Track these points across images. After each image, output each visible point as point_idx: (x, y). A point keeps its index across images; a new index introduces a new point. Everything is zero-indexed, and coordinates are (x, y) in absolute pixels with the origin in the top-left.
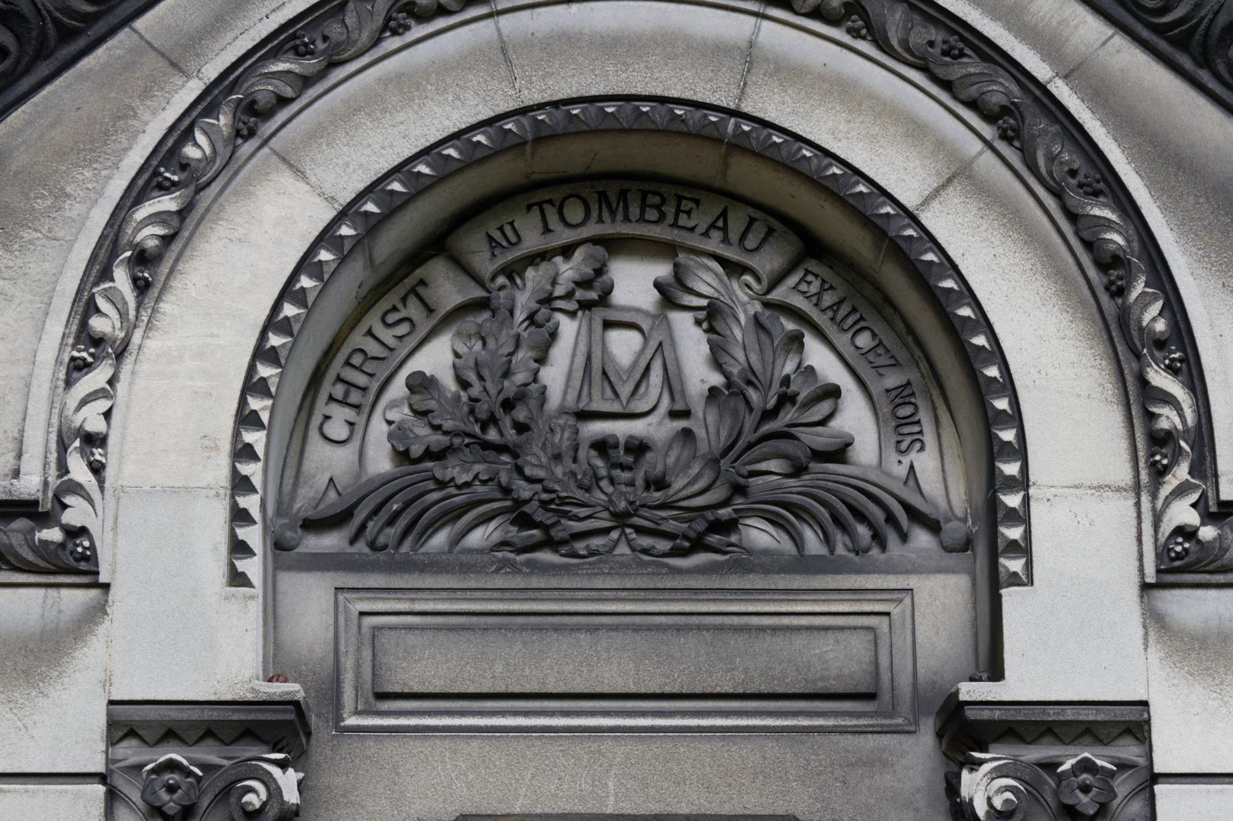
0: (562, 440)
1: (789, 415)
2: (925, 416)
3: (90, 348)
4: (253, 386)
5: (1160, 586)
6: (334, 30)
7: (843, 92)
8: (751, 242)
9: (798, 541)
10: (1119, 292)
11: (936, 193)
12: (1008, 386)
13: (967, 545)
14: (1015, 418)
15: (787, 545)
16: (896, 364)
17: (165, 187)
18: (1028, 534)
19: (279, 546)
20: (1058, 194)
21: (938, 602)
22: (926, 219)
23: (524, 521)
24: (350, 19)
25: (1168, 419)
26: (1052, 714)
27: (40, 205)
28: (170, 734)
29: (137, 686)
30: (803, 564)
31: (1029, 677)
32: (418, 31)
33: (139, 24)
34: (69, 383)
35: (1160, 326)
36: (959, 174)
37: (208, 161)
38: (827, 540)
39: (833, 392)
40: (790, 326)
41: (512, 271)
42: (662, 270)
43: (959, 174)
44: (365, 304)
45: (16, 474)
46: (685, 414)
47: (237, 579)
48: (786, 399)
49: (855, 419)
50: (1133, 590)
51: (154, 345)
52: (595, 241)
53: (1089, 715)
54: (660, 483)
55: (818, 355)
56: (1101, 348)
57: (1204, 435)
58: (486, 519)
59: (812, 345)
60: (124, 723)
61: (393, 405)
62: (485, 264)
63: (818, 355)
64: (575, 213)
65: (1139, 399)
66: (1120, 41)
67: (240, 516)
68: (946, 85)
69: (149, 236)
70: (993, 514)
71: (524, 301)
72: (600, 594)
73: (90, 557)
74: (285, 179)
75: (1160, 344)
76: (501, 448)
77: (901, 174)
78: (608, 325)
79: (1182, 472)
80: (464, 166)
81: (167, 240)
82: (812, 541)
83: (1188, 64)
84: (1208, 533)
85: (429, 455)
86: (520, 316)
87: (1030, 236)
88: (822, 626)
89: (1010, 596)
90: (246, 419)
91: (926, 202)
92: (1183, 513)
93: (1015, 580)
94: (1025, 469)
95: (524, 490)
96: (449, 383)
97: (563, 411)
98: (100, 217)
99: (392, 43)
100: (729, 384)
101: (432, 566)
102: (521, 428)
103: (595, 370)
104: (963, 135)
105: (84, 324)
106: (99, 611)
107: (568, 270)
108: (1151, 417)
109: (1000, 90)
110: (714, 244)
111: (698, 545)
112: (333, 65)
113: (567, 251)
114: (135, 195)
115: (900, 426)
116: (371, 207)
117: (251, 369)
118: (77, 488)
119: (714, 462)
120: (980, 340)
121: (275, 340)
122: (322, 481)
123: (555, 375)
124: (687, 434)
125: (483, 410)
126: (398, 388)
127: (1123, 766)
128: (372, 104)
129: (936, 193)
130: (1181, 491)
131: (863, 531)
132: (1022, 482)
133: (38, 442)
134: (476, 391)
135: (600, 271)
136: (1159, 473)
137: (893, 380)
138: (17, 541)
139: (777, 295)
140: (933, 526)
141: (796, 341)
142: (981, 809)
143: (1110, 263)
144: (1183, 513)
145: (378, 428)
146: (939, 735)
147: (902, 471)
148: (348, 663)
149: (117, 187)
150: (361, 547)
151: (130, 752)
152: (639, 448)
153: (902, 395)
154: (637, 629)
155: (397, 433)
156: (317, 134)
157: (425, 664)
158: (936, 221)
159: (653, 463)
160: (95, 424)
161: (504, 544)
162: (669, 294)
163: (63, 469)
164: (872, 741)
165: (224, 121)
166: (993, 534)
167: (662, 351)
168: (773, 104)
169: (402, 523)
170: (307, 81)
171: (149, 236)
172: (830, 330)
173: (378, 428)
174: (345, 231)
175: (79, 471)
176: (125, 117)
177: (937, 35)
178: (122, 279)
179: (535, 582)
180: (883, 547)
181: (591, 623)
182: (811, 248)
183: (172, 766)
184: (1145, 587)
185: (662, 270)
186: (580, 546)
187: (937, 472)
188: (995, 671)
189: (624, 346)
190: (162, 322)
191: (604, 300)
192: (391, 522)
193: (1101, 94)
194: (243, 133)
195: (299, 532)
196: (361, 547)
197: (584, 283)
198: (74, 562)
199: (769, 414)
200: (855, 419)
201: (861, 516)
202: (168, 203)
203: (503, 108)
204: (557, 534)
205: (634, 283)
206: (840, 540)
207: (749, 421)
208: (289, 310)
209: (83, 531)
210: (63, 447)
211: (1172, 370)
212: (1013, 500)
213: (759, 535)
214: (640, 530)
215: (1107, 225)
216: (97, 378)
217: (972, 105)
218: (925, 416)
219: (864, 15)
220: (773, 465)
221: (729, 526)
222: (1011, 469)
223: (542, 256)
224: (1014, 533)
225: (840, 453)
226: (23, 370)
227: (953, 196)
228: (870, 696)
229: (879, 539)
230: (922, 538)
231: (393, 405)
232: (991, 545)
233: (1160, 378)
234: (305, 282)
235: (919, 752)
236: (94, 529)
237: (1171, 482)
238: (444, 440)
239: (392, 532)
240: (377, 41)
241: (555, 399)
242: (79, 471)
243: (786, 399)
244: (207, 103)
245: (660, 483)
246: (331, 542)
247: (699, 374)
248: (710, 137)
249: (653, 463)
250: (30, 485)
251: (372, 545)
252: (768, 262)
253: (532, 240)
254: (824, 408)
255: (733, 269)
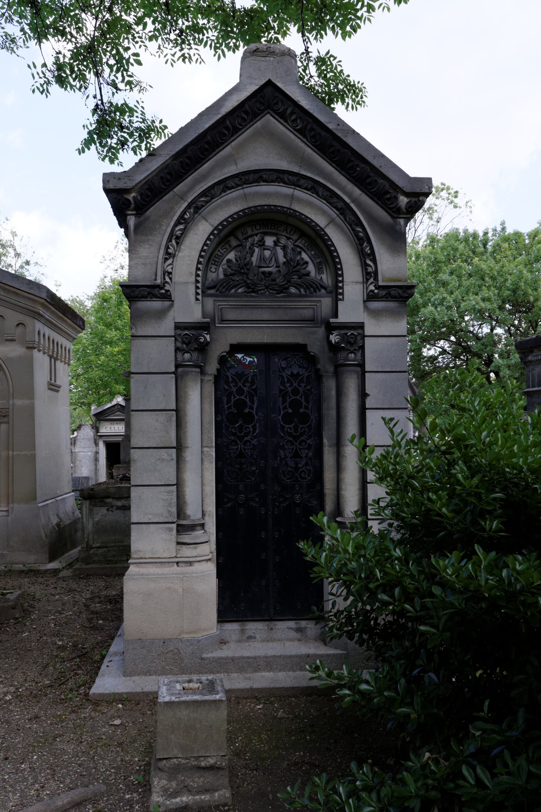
0: (256, 272)
1: (299, 267)
2: (324, 267)
3: (169, 256)
4: (199, 262)
5: (367, 301)
6: (213, 192)
7: (310, 204)
8: (292, 233)
9: (300, 291)
10: (362, 245)
11: (328, 225)
12: (340, 263)
13: (331, 292)
14: (341, 269)
15: (298, 292)
16: (319, 257)
17: (181, 224)
18: (343, 291)
19: (203, 292)
20: (351, 225)
21: (326, 302)
22: (326, 230)
23: (249, 288)
24: (216, 190)
25: (370, 269)
26: (347, 325)
27: (157, 227)
28: (186, 328)
29: (181, 319)
30: (301, 296)
31: (344, 317)
32: (228, 192)
33: (175, 190)
34: (165, 262)
35: (369, 252)
36: (332, 221)
37: (189, 218)
38: (306, 291)
39: (307, 263)
40: (299, 250)
41: (246, 239)
42: (274, 238)
43: (332, 221)
44: (218, 245)
45: (156, 280)
46: (279, 267)
47: (197, 299)
48: (298, 264)
49: (311, 268)
50: (362, 302)
51: (180, 254)
52: (262, 233)
53: (353, 325)
54: (274, 280)
55: (304, 256)
56: (358, 259)
57: (376, 273)
58: (241, 287)
59: (303, 253)
60: (178, 326)
61: (224, 265)
62: (241, 237)
63: (304, 256)
64: (258, 227)
65: (364, 266)
66: (363, 195)
67: (197, 288)
68: (330, 203)
69: (179, 233)
70: (337, 287)
71: (248, 245)
72: (263, 301)
73: (170, 296)
74: (204, 222)
75: (369, 255)
76: (244, 273)
77: (321, 221)
78: (264, 249)
79: (372, 280)
80: (237, 219)
81: (182, 234)
82: (302, 291)
83: (376, 199)
84: (376, 291)
85: (231, 275)
86: (247, 247)
87: (345, 234)
88: (304, 308)
89: (340, 303)
90: (198, 269)
91: (326, 227)
92: (372, 287)
93: (340, 300)
94: (343, 279)
95: (249, 282)
96: (234, 260)
97: (256, 266)
98: (169, 230)
99: (223, 194)
100: (287, 261)
101: (232, 296)
102: (248, 269)
103: (262, 258)
104: (333, 213)
105: (167, 251)
106: (172, 306)
107: (256, 239)
108: (367, 269)
109: (340, 205)
110: (284, 234)
111: (281, 292)
112: (212, 198)
113: (256, 235)
114: (176, 225)
115: (319, 270)
116: (220, 227)
117: (198, 259)
118: (167, 283)
119: (284, 276)
120: (335, 254)
121: (203, 254)
122: (210, 280)
123: (254, 259)
124: (279, 271)
125: (241, 266)
126: (225, 261)
127: (359, 334)
128: (220, 207)
129: (328, 225)
130: (372, 283)
131: (312, 289)
132: (342, 281)
133: (159, 273)
134: (239, 262)
135: (263, 239)
136: (368, 280)
137: (318, 260)
138: (156, 292)
139: (296, 244)
140: (325, 288)
141: (300, 253)
142: (333, 342)
143: (360, 239)
144: (372, 287)
145: (221, 269)
146: (325, 328)
147: (319, 278)
148: (216, 314)
149: (172, 224)
150: (218, 292)
151: (179, 332)
152: (270, 273)
153: (320, 263)
154: (270, 308)
155: (224, 270)
156: (210, 212)
157: (231, 315)
158: (328, 231)
159: (273, 276)
160: (170, 270)
161: (245, 292)
162: (276, 243)
163: (164, 279)
164: (313, 329)
165: (192, 210)
166: (337, 291)
167: (274, 254)
168: (297, 207)
169: (226, 288)
170: (207, 202)
171: (179, 233)
172: (307, 251)
173: (221, 269)
174: (215, 232)
175: (167, 279)
176: (172, 210)
177: (328, 193)
178: (174, 242)
179: (251, 299)
180: (316, 292)
181: (262, 307)
182: (303, 234)
183: (186, 334)
184: (364, 301)
185: (274, 238)
186: (259, 292)
187: (326, 278)
188: (336, 316)
189: (267, 253)
190: (181, 250)
191: (264, 244)
192: (224, 288)
193: (359, 205)
194: (196, 212)
195: (206, 289)
196: (218, 292)
197: (259, 241)
198: (167, 296)
199: (295, 267)
200: (311, 268)
201: (312, 287)
202: (182, 227)
203: (245, 207)
204: (255, 290)
205: (269, 241)
206: (308, 291)
207: (291, 268)
208: (205, 248)
209: (169, 291)
210: (164, 275)
211: (371, 260)
212: (340, 285)
213: (293, 290)
214: (271, 289)
215: (360, 232)
216: (170, 261)
217: (335, 207)
218: (324, 267)
219: (315, 189)
220: (296, 277)
221: (287, 288)
222: (340, 279)
223: (251, 236)
224: (341, 291)
225: (308, 274)
226: (155, 259)
227: (331, 226)
228: (313, 321)
229: (315, 291)
230: (323, 291)
231: (224, 265)
232: (336, 293)
233: (369, 262)
234: (208, 242)
235: (321, 331)
236: (171, 290)
237: (370, 282)
238: (232, 272)
239: (224, 290)
240: (221, 194)
241: (254, 264)
242: (167, 279)
243: (298, 264)
244: (189, 207)
245: (274, 280)
246: (212, 291)
247: (282, 259)
248: (285, 213)
249: (273, 276)
250: (159, 281)
251: (220, 292)
252: (295, 237)
253: (250, 233)
254: (305, 266)
255: (288, 238)
